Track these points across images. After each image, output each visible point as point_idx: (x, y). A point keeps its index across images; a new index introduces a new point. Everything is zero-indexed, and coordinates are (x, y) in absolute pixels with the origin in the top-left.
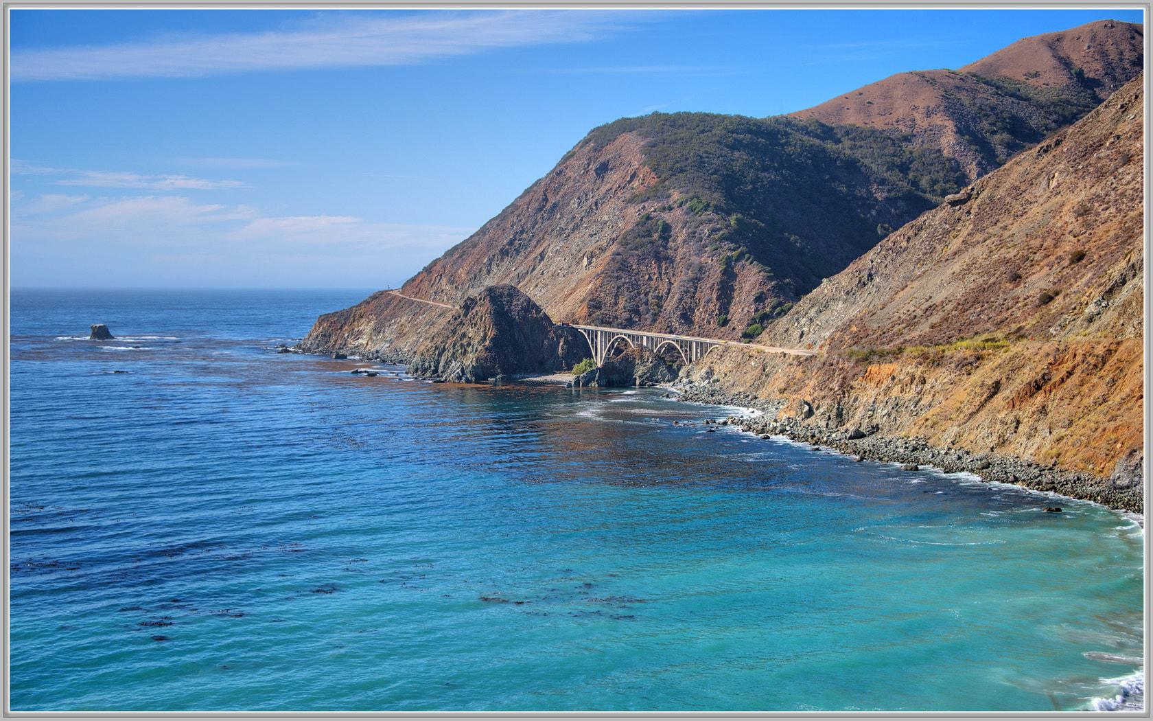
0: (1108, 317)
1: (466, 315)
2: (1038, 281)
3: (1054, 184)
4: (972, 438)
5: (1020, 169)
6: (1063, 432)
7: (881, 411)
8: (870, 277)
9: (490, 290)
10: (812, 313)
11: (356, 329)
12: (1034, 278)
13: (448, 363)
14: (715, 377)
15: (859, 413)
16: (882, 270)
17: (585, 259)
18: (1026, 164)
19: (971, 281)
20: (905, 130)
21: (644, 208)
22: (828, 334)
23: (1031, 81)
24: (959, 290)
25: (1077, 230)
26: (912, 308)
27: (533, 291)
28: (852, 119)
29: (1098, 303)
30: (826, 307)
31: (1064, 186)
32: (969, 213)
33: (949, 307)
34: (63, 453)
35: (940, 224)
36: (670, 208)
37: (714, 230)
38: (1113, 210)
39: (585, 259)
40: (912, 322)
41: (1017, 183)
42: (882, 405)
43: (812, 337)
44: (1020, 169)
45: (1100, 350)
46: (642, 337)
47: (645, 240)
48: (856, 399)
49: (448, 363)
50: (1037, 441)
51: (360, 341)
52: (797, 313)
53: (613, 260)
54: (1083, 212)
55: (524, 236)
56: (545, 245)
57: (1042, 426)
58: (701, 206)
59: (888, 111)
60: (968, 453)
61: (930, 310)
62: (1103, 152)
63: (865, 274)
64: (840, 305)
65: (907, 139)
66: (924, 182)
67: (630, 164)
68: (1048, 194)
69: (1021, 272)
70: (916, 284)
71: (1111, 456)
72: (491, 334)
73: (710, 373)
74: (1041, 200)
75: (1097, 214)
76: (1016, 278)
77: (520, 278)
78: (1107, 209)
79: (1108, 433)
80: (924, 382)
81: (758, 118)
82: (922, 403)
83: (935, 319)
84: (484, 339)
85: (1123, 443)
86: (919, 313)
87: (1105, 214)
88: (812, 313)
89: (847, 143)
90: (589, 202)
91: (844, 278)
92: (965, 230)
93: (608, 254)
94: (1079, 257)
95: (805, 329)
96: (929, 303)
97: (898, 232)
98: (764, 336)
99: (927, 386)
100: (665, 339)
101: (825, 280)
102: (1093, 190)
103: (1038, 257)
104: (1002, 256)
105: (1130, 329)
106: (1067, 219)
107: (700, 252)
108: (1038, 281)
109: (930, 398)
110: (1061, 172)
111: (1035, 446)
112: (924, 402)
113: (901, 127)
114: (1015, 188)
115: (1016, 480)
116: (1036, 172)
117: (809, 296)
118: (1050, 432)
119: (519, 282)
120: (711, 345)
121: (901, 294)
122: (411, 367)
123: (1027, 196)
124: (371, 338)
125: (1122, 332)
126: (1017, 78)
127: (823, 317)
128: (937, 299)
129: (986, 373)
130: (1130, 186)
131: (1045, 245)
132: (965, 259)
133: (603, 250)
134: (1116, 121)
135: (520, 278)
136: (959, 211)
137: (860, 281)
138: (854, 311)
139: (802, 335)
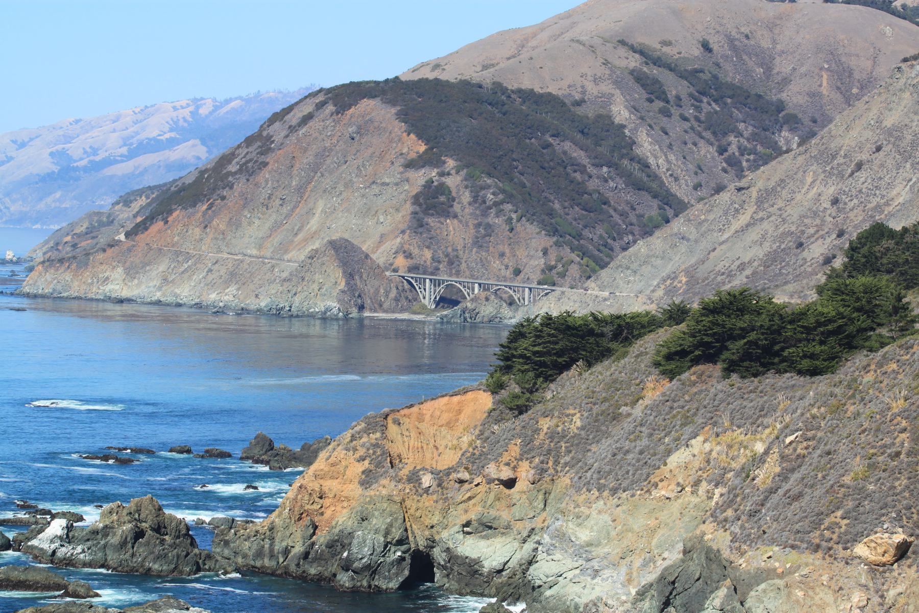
19: (767, 247)
20: (578, 97)
23: (666, 49)
24: (759, 252)
25: (834, 214)
26: (727, 265)
33: (756, 264)
38: (855, 201)
41: (783, 178)
46: (425, 279)
61: (742, 267)
65: (578, 103)
70: (723, 247)
71: (699, 596)
78: (852, 200)
83: (748, 272)
87: (851, 204)
92: (750, 210)
104: (787, 230)
106: (825, 205)
113: (574, 93)
121: (712, 255)
126: (654, 46)
136: (743, 196)
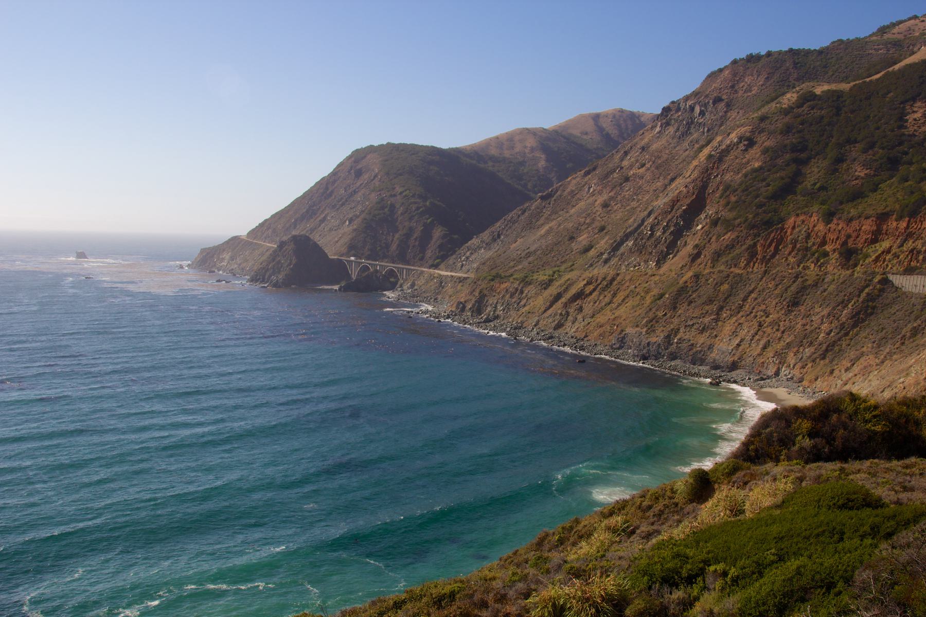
0: (614, 261)
1: (280, 251)
2: (583, 239)
3: (592, 190)
4: (545, 322)
5: (574, 182)
6: (590, 320)
7: (500, 308)
8: (499, 236)
9: (294, 237)
10: (468, 253)
11: (221, 257)
12: (581, 239)
13: (270, 276)
14: (416, 287)
15: (489, 309)
16: (504, 232)
17: (347, 221)
18: (578, 179)
21: (380, 194)
22: (475, 265)
27: (316, 238)
28: (494, 152)
29: (609, 253)
30: (475, 251)
31: (596, 191)
32: (549, 204)
33: (539, 252)
34: (143, 504)
35: (535, 209)
36: (395, 196)
37: (418, 208)
38: (619, 205)
39: (347, 221)
40: (520, 261)
42: (500, 305)
43: (467, 267)
44: (574, 182)
45: (609, 278)
47: (381, 212)
48: (487, 301)
49: (270, 276)
50: (577, 325)
51: (223, 263)
52: (460, 254)
53: (362, 222)
54: (605, 205)
55: (315, 208)
56: (326, 213)
57: (580, 317)
58: (411, 194)
59: (513, 148)
60: (542, 331)
62: (615, 175)
63: (496, 234)
64: (483, 251)
66: (530, 186)
67: (373, 170)
68: (588, 195)
69: (575, 235)
72: (294, 262)
73: (413, 285)
74: (585, 198)
75: (612, 207)
76: (572, 238)
77: (312, 230)
79: (610, 321)
80: (522, 292)
81: (443, 148)
82: (521, 304)
84: (290, 264)
85: (617, 327)
86: (523, 255)
87: (616, 208)
88: (468, 253)
89: (490, 164)
90: (351, 191)
91: (486, 235)
93: (359, 220)
94: (602, 229)
95: (464, 263)
96: (528, 251)
97: (513, 212)
98: (442, 266)
99: (524, 295)
100: (388, 266)
101: (475, 236)
102: (610, 194)
103: (583, 228)
105: (623, 267)
107: (411, 219)
108: (583, 239)
109: (525, 300)
110: (595, 185)
111: (576, 328)
112: (522, 303)
114: (573, 191)
115: (565, 345)
116: (583, 183)
117: (466, 245)
118: (583, 320)
119: (311, 233)
120: (414, 270)
122: (625, 168)
123: (578, 196)
124: (229, 262)
125: (619, 269)
127: (473, 256)
128: (532, 249)
129: (553, 290)
130: (628, 193)
131: (587, 222)
132: (547, 227)
133: (357, 217)
134: (622, 160)
135: (312, 230)
137: (493, 238)
138: (490, 254)
139: (462, 266)
